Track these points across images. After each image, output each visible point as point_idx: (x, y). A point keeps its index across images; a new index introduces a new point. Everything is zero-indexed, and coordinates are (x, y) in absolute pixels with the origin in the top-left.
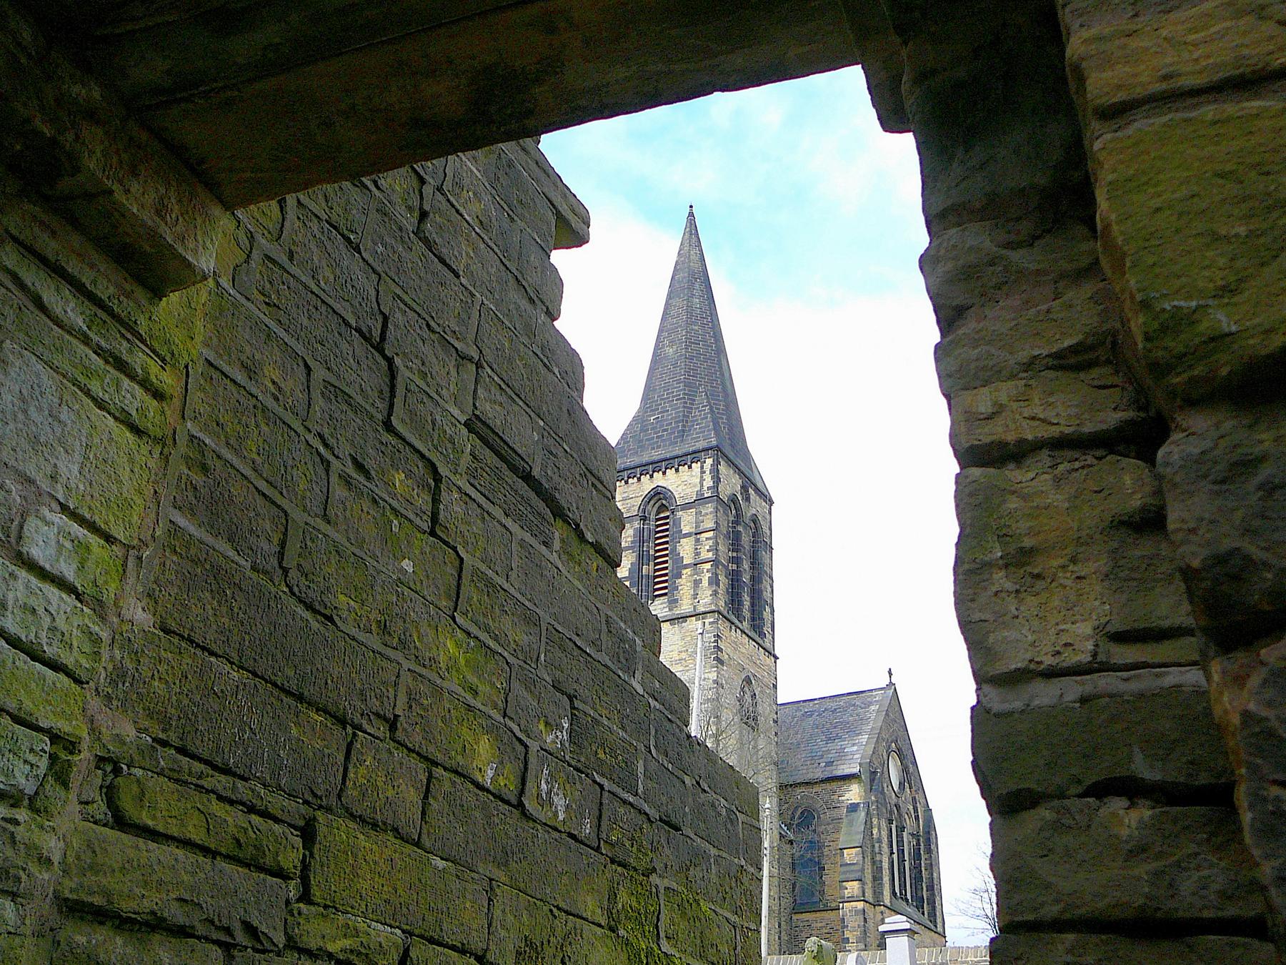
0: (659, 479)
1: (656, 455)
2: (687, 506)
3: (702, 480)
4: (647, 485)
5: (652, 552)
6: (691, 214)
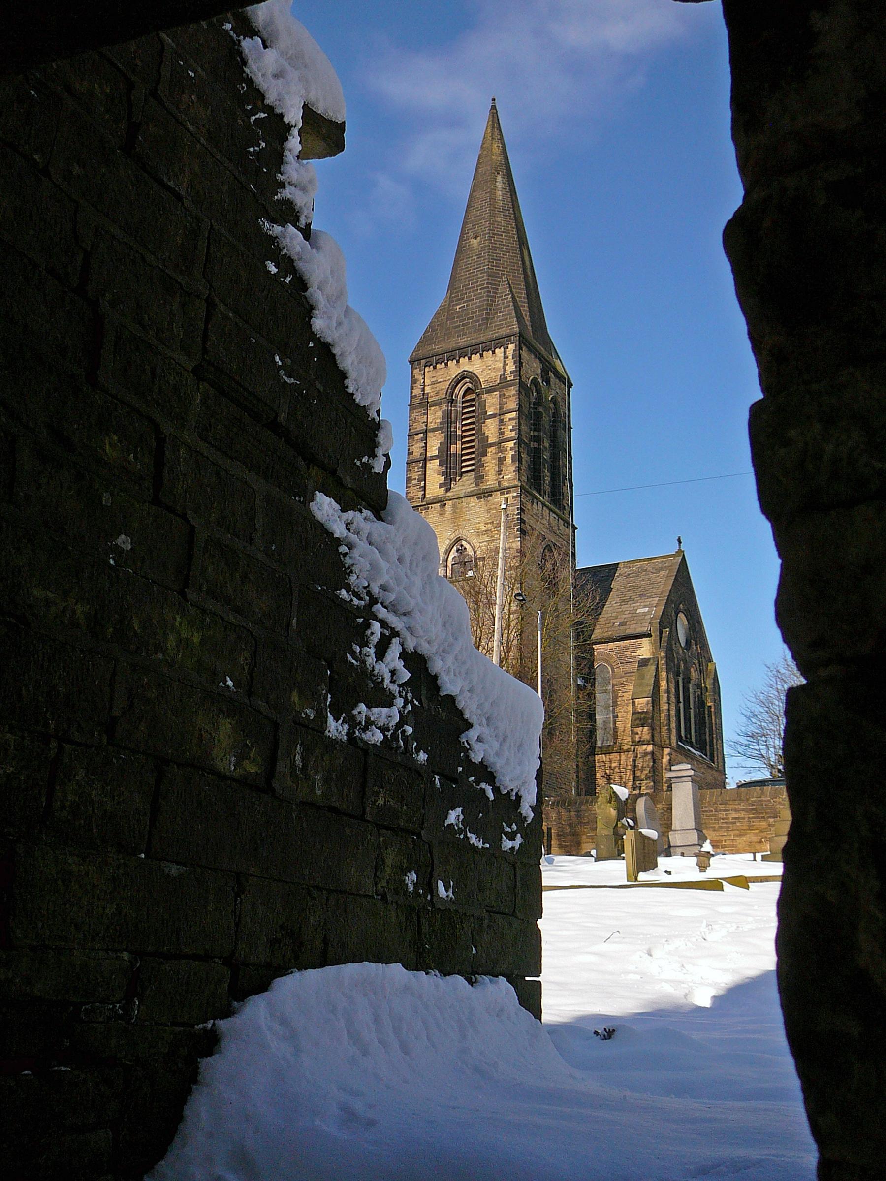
0: (465, 365)
3: (505, 364)
6: (494, 107)
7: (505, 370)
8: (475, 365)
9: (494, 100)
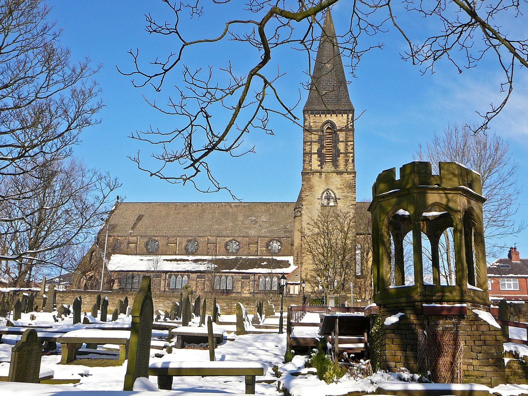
0: (329, 117)
2: (341, 130)
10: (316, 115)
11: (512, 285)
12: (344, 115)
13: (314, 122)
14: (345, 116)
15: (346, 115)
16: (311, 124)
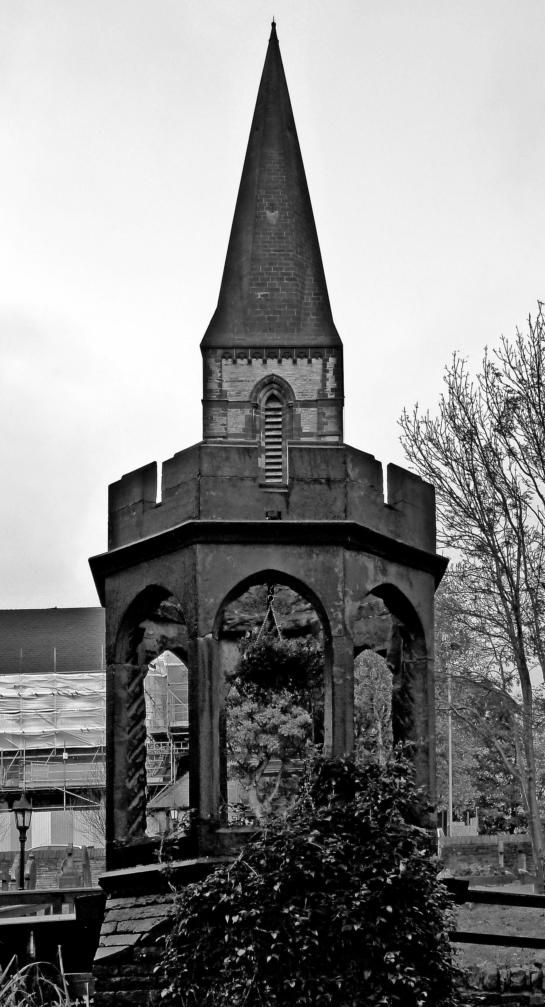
0: (273, 367)
1: (297, 340)
2: (306, 404)
3: (324, 380)
4: (260, 370)
5: (263, 444)
6: (274, 41)
7: (324, 385)
8: (285, 370)
9: (274, 25)
10: (239, 361)
11: (4, 758)
12: (314, 360)
13: (233, 381)
14: (317, 363)
15: (320, 361)
16: (225, 386)
